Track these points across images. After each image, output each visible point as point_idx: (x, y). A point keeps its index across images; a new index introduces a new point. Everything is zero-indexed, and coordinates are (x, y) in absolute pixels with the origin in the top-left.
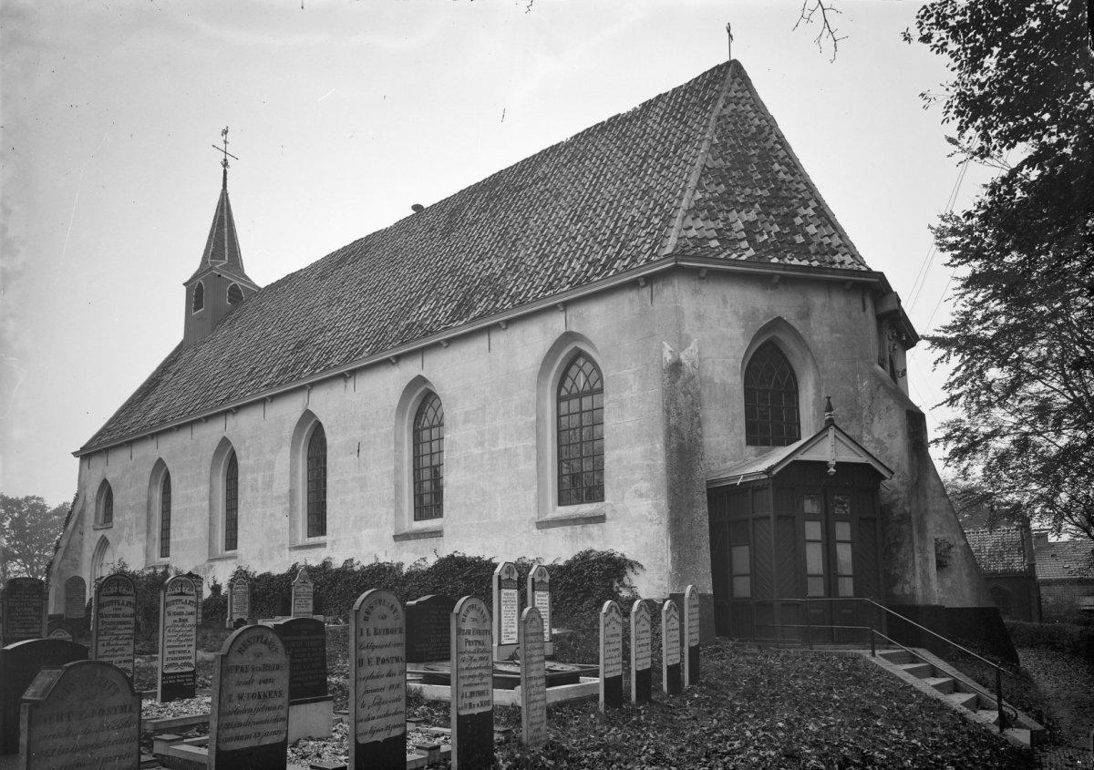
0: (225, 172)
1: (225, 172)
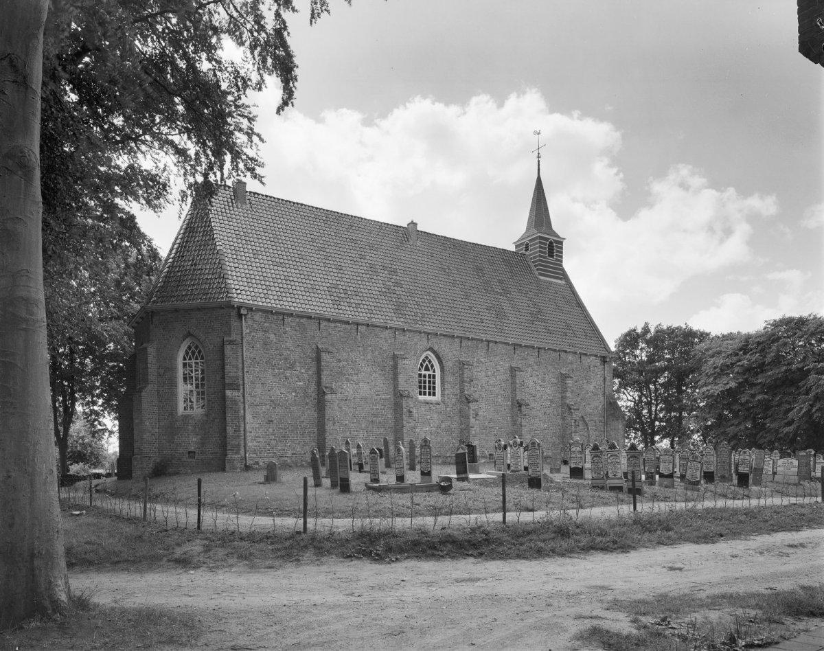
0: (539, 161)
1: (539, 161)
